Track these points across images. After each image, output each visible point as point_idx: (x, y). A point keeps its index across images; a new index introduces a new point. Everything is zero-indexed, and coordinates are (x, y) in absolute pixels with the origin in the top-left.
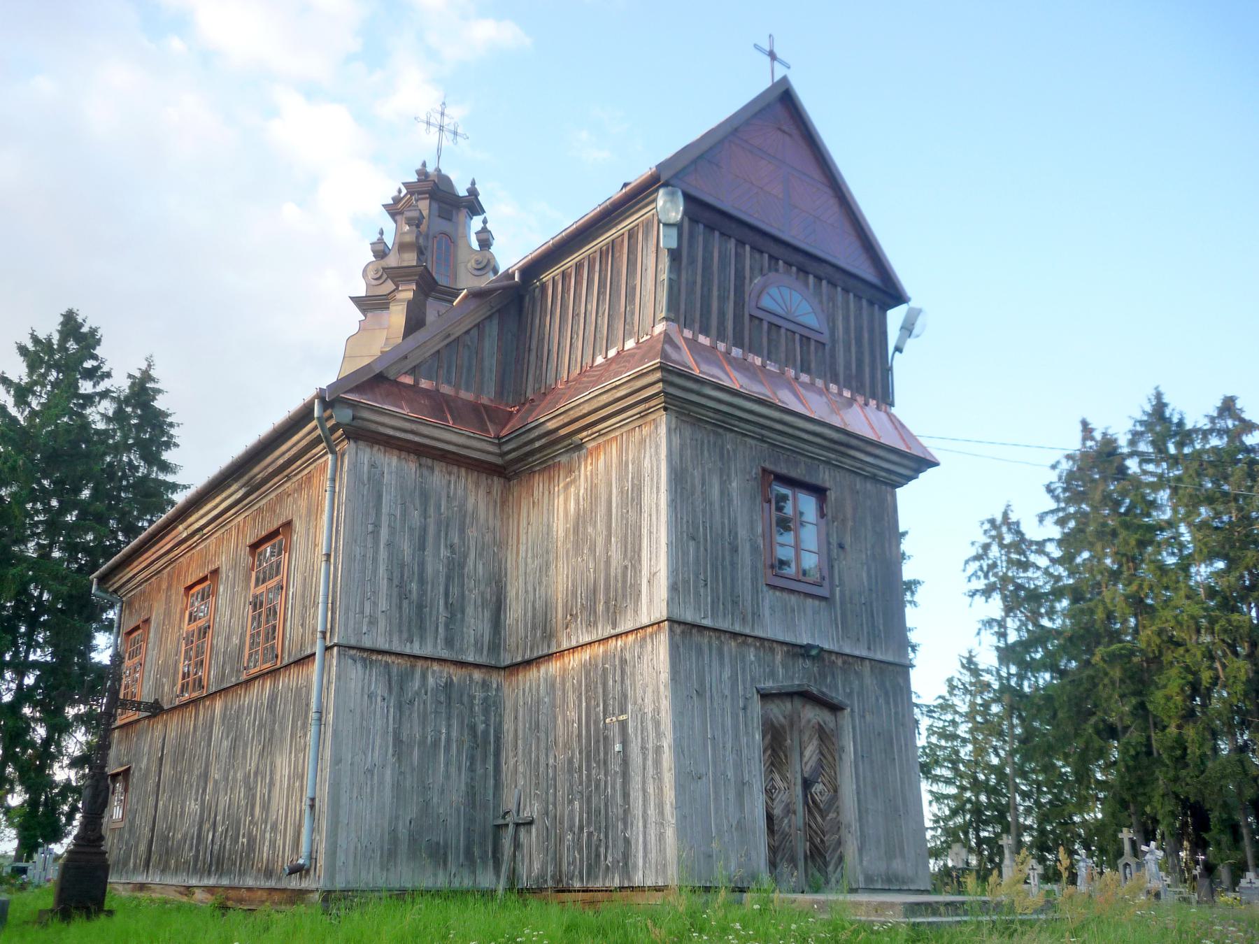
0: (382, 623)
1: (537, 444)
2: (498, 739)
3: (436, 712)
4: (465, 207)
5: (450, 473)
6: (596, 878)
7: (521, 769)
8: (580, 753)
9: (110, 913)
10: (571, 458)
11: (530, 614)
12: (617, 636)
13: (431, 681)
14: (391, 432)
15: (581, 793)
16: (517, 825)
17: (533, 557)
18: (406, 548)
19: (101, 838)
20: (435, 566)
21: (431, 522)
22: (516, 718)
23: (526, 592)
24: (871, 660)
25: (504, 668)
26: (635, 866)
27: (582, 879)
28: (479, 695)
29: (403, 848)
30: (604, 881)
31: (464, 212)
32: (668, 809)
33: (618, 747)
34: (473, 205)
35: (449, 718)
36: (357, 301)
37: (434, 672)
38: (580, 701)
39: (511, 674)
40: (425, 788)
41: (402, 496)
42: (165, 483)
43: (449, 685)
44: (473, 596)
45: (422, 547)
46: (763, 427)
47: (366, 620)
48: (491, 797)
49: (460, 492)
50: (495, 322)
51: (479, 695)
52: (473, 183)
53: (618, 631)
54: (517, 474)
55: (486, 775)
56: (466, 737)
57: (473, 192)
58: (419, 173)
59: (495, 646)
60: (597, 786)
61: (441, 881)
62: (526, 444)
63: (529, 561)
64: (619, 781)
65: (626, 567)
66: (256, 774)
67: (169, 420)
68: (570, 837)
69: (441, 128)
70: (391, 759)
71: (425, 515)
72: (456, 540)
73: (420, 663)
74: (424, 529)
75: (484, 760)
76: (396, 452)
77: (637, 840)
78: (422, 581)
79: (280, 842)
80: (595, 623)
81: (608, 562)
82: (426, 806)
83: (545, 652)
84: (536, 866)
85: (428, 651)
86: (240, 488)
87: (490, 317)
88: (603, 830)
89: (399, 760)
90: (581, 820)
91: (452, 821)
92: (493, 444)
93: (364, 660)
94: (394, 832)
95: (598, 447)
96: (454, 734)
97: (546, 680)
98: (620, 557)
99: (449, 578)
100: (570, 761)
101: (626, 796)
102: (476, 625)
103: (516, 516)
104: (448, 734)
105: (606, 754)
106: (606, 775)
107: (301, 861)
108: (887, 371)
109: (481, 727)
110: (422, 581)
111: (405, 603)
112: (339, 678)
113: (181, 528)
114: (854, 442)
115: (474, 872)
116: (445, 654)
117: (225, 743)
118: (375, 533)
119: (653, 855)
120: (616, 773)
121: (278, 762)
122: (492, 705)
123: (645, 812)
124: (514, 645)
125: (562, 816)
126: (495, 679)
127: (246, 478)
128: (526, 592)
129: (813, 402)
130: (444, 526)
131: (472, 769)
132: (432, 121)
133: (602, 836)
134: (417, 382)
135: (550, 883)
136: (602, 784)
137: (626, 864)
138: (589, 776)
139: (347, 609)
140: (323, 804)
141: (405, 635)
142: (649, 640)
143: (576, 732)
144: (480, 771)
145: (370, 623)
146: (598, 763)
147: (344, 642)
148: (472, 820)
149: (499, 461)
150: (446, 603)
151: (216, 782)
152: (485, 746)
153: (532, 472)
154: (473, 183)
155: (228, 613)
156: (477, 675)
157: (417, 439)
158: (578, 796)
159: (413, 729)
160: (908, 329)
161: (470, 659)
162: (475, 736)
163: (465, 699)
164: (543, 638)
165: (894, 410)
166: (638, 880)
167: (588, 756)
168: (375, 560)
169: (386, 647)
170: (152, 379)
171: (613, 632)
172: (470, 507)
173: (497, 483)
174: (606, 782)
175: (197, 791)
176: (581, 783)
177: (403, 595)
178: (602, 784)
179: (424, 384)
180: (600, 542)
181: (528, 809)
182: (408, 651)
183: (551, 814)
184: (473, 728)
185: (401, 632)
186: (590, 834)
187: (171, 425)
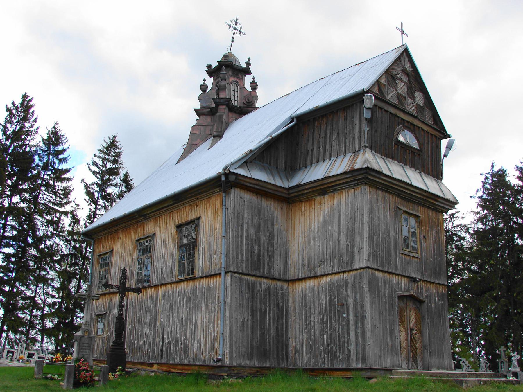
1: (306, 192)
2: (287, 310)
7: (297, 321)
8: (327, 316)
12: (344, 272)
13: (263, 286)
14: (249, 185)
15: (327, 332)
18: (252, 231)
22: (295, 301)
29: (255, 351)
33: (345, 315)
36: (196, 110)
37: (264, 283)
38: (326, 296)
52: (249, 60)
54: (294, 202)
59: (285, 273)
60: (335, 330)
62: (301, 191)
66: (186, 320)
68: (322, 348)
69: (235, 29)
70: (250, 317)
72: (271, 229)
74: (259, 225)
76: (249, 192)
79: (202, 347)
81: (339, 241)
84: (305, 359)
90: (327, 342)
96: (272, 307)
107: (220, 357)
109: (281, 304)
110: (259, 246)
122: (284, 295)
125: (318, 340)
126: (286, 285)
129: (416, 179)
131: (278, 321)
132: (232, 25)
133: (338, 348)
136: (337, 329)
137: (348, 359)
138: (331, 326)
140: (227, 335)
143: (324, 308)
144: (280, 322)
148: (278, 342)
149: (287, 196)
150: (268, 254)
151: (162, 322)
153: (301, 201)
154: (249, 60)
157: (258, 187)
160: (449, 147)
162: (279, 308)
163: (275, 294)
167: (330, 317)
173: (285, 205)
174: (339, 328)
175: (150, 325)
176: (327, 328)
178: (337, 329)
180: (336, 235)
184: (278, 305)
186: (332, 348)
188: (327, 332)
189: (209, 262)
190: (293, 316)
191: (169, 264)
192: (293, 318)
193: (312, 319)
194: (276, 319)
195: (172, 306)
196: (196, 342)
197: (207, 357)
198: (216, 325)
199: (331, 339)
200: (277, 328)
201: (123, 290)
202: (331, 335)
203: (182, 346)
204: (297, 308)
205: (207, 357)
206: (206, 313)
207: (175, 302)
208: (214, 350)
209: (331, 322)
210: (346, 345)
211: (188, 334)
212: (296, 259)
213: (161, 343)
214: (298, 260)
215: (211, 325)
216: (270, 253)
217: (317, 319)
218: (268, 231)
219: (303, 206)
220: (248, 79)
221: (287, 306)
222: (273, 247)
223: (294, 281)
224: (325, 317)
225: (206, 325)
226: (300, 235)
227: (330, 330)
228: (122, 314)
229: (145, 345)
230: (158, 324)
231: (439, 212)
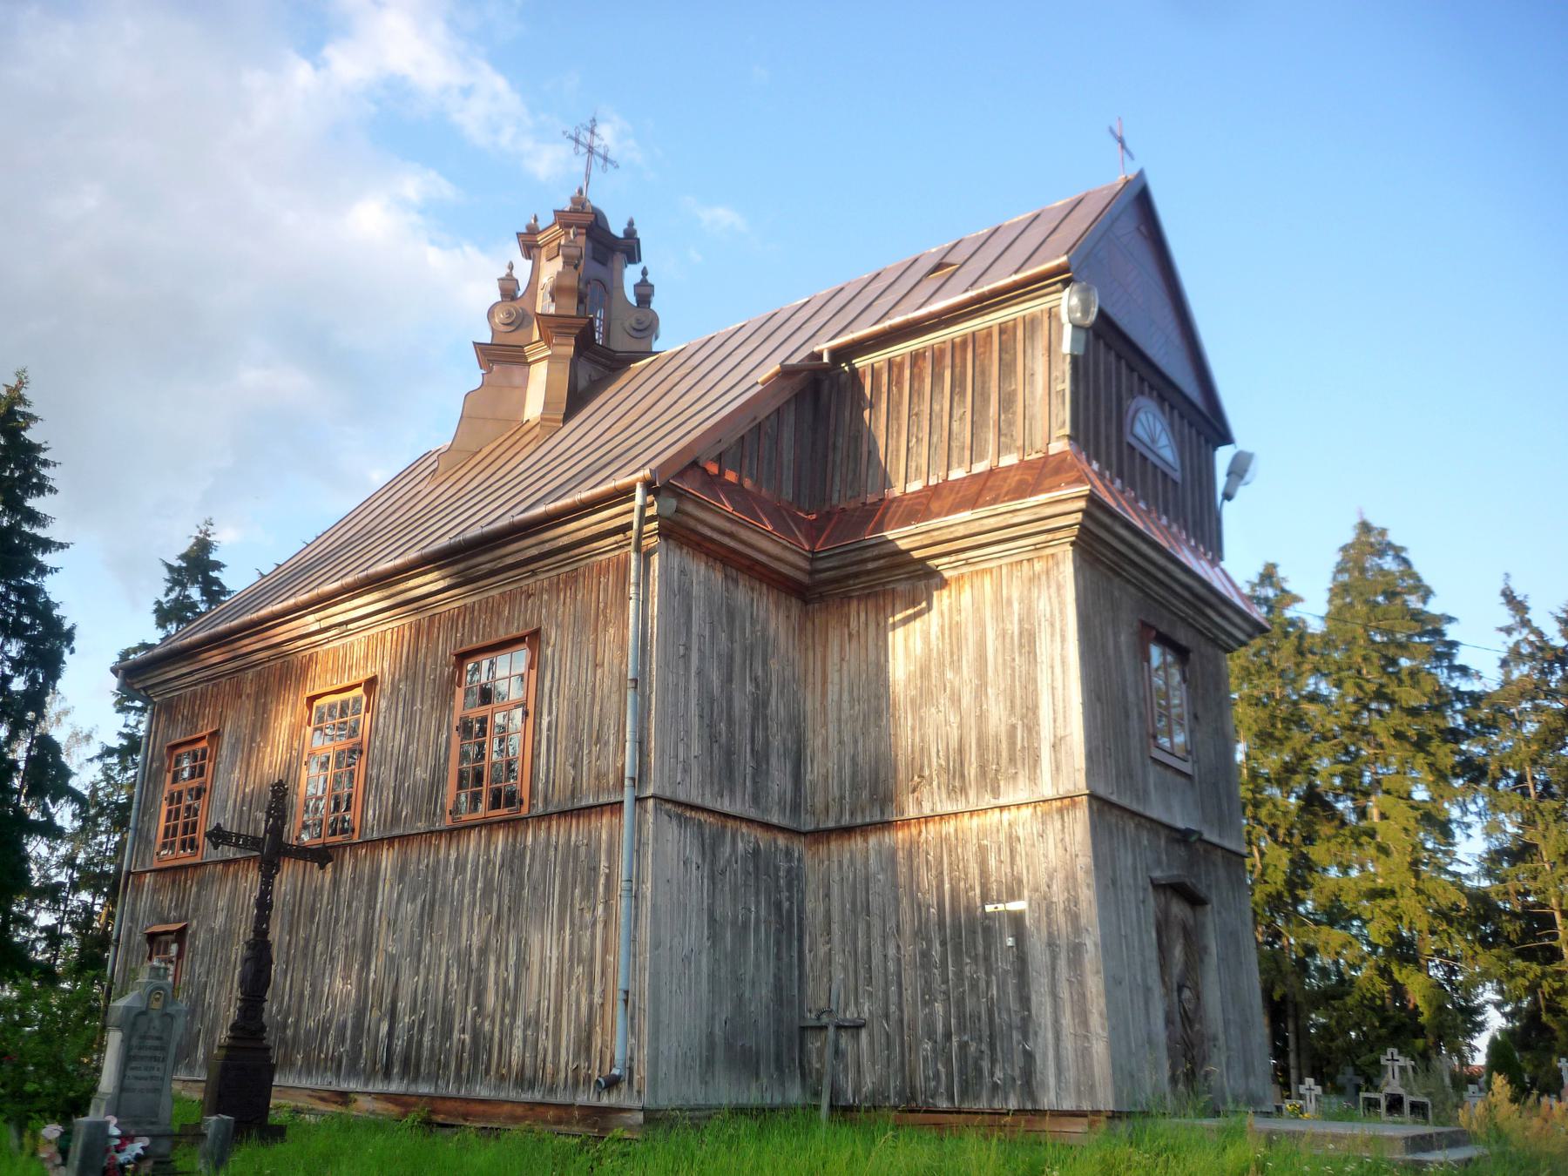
0: (695, 771)
1: (870, 566)
3: (745, 885)
4: (623, 252)
5: (752, 589)
6: (977, 1098)
7: (838, 959)
8: (943, 944)
9: (279, 1132)
10: (915, 588)
11: (847, 770)
14: (709, 533)
15: (946, 993)
16: (839, 1027)
17: (852, 700)
18: (715, 678)
19: (263, 1028)
20: (742, 705)
21: (737, 646)
23: (841, 742)
24: (1223, 848)
25: (805, 834)
26: (1043, 1084)
27: (951, 1098)
28: (783, 865)
29: (720, 1053)
30: (990, 1101)
31: (620, 257)
32: (1096, 1022)
33: (1010, 942)
34: (630, 248)
35: (757, 894)
39: (817, 842)
40: (738, 980)
41: (711, 614)
42: (35, 538)
43: (756, 852)
44: (776, 743)
45: (730, 680)
46: (1147, 573)
47: (680, 766)
48: (796, 992)
49: (762, 613)
50: (793, 407)
51: (783, 865)
53: (1002, 801)
55: (790, 965)
56: (773, 918)
57: (630, 233)
58: (574, 200)
60: (974, 985)
61: (752, 1096)
63: (846, 705)
64: (1012, 982)
65: (1014, 727)
66: (483, 952)
67: (42, 456)
68: (928, 1046)
69: (591, 150)
71: (731, 639)
72: (760, 673)
73: (730, 823)
74: (731, 658)
75: (790, 947)
76: (704, 557)
77: (1045, 1055)
78: (730, 722)
80: (963, 790)
81: (982, 717)
82: (740, 1001)
83: (877, 818)
85: (736, 809)
86: (443, 578)
87: (788, 402)
88: (986, 1039)
89: (714, 945)
90: (947, 1025)
91: (762, 1023)
92: (806, 557)
93: (679, 816)
94: (711, 1034)
95: (960, 578)
96: (763, 913)
97: (879, 853)
98: (1004, 715)
99: (754, 719)
100: (925, 955)
101: (1025, 1001)
102: (779, 779)
103: (819, 649)
104: (757, 912)
105: (988, 947)
106: (988, 973)
107: (616, 1072)
108: (1219, 521)
109: (786, 905)
110: (730, 722)
111: (716, 746)
112: (656, 839)
113: (311, 618)
114: (1213, 600)
115: (783, 1084)
116: (752, 813)
117: (408, 908)
118: (686, 657)
119: (1071, 1075)
120: (1006, 972)
121: (535, 939)
122: (795, 878)
123: (1056, 1021)
124: (820, 806)
125: (914, 1020)
126: (798, 846)
127: (461, 566)
128: (841, 742)
130: (749, 651)
131: (778, 957)
133: (984, 1047)
134: (721, 473)
135: (893, 1100)
136: (982, 985)
138: (959, 974)
139: (663, 752)
141: (716, 788)
142: (1056, 817)
145: (685, 771)
146: (975, 959)
147: (659, 793)
148: (779, 1021)
150: (752, 750)
151: (391, 958)
152: (788, 926)
153: (846, 598)
155: (400, 737)
156: (781, 841)
157: (732, 544)
158: (940, 997)
159: (725, 908)
160: (1239, 470)
161: (775, 820)
162: (781, 916)
164: (872, 801)
165: (1223, 564)
166: (1048, 1101)
168: (687, 689)
169: (698, 801)
170: (22, 400)
171: (994, 802)
172: (772, 632)
173: (795, 604)
175: (348, 967)
176: (945, 981)
177: (713, 738)
178: (982, 985)
179: (731, 476)
181: (852, 1007)
182: (718, 807)
183: (894, 1017)
184: (778, 905)
185: (712, 783)
186: (963, 1046)
187: (45, 463)
188: (946, 993)
189: (574, 766)
190: (821, 940)
191: (421, 774)
192: (822, 950)
193: (892, 951)
194: (773, 950)
195: (432, 905)
196: (519, 1022)
197: (562, 1075)
198: (598, 969)
199: (961, 1017)
200: (777, 978)
201: (271, 851)
202: (961, 1002)
203: (467, 1037)
204: (836, 916)
205: (562, 1075)
206: (561, 928)
207: (444, 895)
208: (588, 1049)
209: (959, 963)
210: (1016, 1036)
211: (491, 1000)
212: (832, 765)
213: (384, 1027)
214: (840, 769)
215: (579, 970)
216: (758, 747)
217: (908, 950)
218: (755, 680)
219: (853, 613)
220: (631, 275)
221: (801, 911)
222: (766, 728)
223: (820, 835)
224: (937, 945)
225: (598, 970)
226: (846, 697)
227: (957, 986)
228: (266, 932)
229: (326, 1032)
230: (378, 962)
231: (1221, 647)
